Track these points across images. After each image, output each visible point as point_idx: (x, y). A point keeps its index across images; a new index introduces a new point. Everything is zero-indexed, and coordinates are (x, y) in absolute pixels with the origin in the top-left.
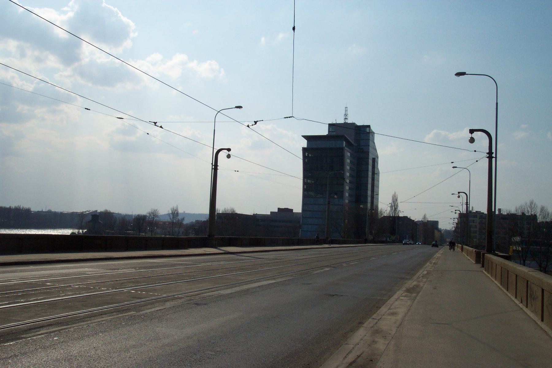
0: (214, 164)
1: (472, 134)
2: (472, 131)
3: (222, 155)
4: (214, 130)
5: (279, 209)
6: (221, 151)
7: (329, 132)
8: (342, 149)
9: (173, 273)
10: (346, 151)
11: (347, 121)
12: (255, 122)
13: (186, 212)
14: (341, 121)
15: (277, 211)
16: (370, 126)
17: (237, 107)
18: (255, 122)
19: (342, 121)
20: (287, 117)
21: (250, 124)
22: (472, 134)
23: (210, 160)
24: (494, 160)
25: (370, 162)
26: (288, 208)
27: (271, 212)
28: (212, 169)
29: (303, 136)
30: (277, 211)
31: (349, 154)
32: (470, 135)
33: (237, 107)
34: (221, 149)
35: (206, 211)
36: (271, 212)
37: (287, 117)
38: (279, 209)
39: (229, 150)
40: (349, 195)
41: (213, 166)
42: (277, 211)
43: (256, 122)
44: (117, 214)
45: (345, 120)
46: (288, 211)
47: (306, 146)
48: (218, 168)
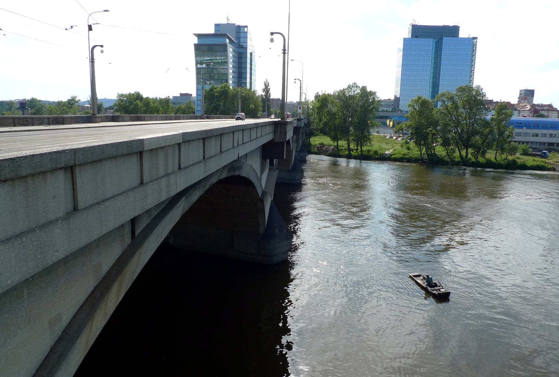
0: (91, 58)
1: (272, 35)
2: (272, 34)
3: (97, 50)
4: (289, 13)
5: (181, 94)
6: (96, 47)
7: (215, 31)
8: (225, 46)
9: (535, 200)
10: (228, 47)
11: (229, 22)
12: (71, 26)
13: (107, 98)
14: (224, 22)
15: (179, 95)
16: (247, 26)
17: (105, 11)
18: (71, 26)
19: (226, 22)
20: (95, 24)
21: (68, 28)
22: (272, 35)
23: (87, 55)
24: (286, 55)
25: (249, 56)
26: (188, 93)
27: (173, 97)
28: (90, 62)
29: (194, 34)
30: (179, 96)
31: (231, 50)
32: (271, 37)
33: (105, 11)
34: (94, 46)
35: (299, 101)
36: (173, 97)
37: (95, 24)
38: (181, 94)
39: (102, 46)
40: (232, 82)
41: (91, 60)
42: (179, 95)
43: (72, 27)
44: (45, 101)
45: (228, 21)
46: (188, 95)
47: (196, 43)
48: (95, 61)
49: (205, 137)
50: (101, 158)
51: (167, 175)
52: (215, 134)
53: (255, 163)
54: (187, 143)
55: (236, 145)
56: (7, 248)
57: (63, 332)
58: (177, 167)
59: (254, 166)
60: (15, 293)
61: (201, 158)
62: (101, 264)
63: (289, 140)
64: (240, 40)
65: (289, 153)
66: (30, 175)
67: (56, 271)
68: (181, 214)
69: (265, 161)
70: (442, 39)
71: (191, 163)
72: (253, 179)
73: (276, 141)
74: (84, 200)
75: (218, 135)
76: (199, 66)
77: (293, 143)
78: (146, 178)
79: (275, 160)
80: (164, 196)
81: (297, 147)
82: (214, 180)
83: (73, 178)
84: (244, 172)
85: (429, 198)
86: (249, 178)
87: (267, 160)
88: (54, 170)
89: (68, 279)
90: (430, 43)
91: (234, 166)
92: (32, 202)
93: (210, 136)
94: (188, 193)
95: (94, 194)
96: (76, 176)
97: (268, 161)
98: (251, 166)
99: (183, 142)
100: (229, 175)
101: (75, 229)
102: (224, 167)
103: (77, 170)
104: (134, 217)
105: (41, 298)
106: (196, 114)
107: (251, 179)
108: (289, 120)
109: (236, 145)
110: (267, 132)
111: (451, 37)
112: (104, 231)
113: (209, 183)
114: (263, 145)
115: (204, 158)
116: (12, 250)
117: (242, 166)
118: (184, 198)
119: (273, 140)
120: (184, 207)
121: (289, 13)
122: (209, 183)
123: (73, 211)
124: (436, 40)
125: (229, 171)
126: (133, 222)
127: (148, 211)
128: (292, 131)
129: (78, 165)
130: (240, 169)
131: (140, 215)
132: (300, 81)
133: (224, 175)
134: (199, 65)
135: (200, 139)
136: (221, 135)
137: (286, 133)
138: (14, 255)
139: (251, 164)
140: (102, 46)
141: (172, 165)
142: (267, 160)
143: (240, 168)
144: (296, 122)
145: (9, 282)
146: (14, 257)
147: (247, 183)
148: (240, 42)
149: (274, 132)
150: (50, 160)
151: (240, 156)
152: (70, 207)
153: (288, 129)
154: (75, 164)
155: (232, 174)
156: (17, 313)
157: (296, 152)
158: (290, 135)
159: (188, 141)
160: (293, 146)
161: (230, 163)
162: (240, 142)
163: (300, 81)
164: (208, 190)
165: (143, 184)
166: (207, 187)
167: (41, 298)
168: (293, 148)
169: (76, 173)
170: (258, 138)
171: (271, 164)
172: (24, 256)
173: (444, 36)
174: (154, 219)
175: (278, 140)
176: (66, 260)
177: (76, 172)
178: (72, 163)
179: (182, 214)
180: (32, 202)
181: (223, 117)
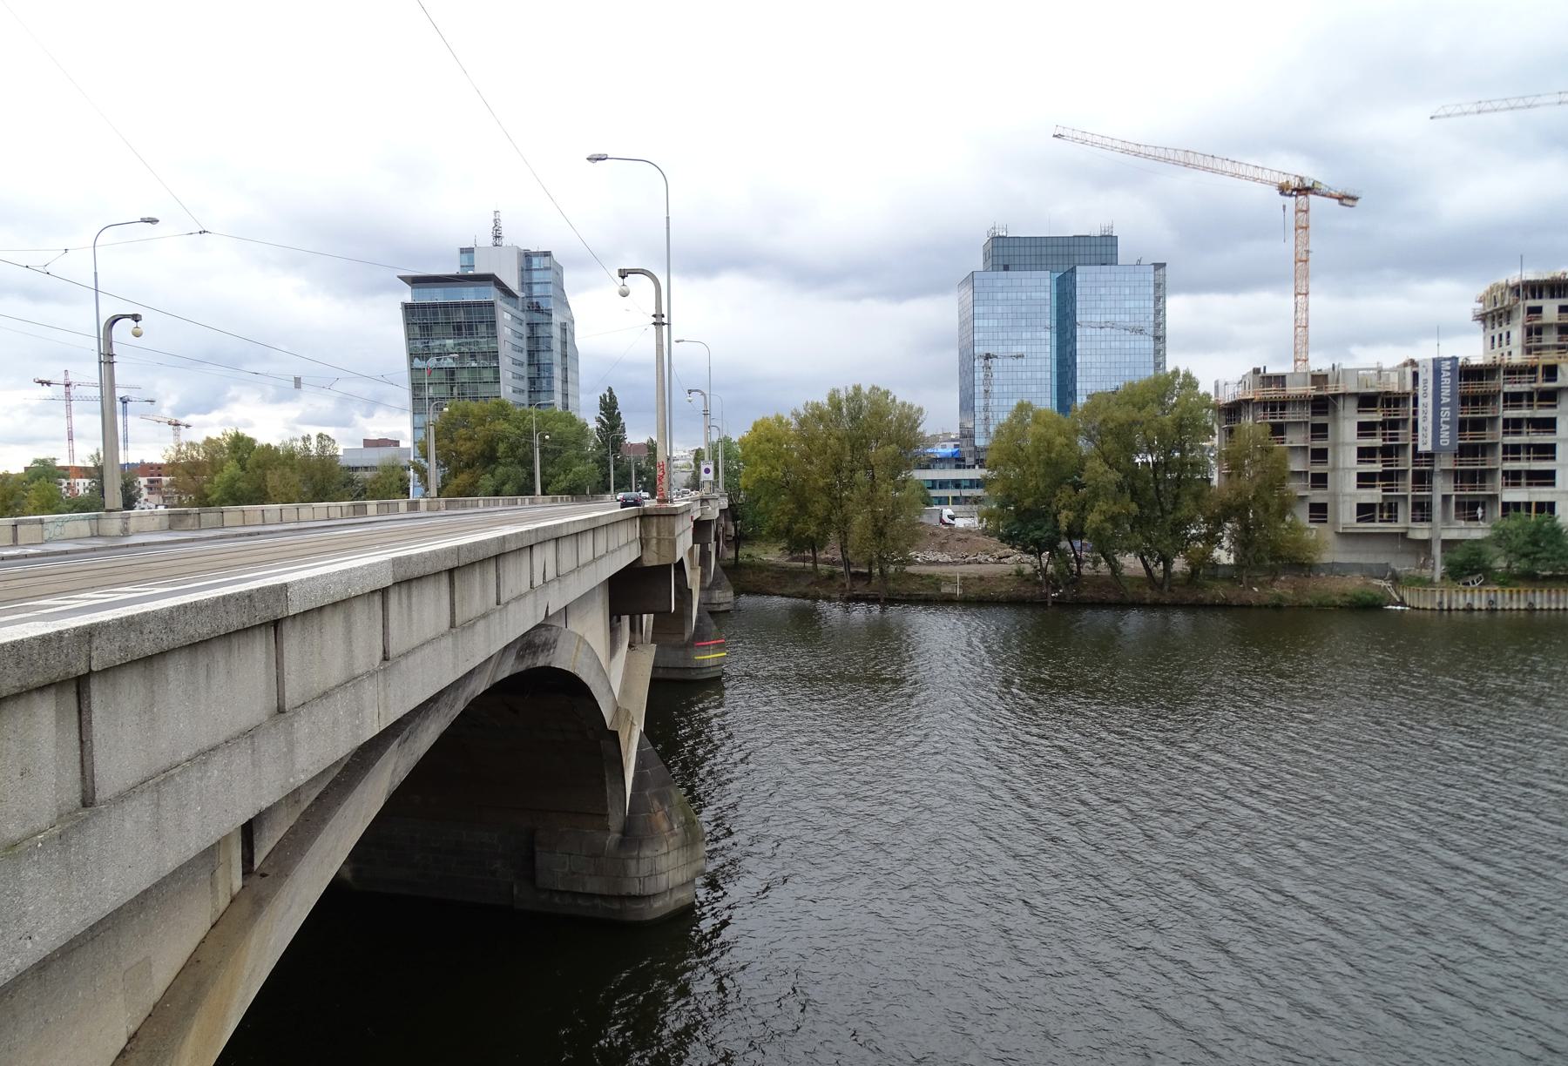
1: (623, 277)
2: (623, 274)
3: (123, 329)
13: (146, 462)
25: (556, 332)
29: (403, 278)
39: (136, 318)
49: (456, 564)
50: (165, 646)
51: (352, 680)
52: (481, 555)
53: (592, 627)
55: (538, 581)
58: (379, 654)
59: (588, 638)
62: (150, 965)
63: (682, 559)
64: (530, 289)
65: (684, 593)
67: (12, 997)
68: (386, 791)
69: (619, 620)
70: (1073, 271)
71: (416, 642)
73: (647, 564)
76: (418, 363)
77: (692, 568)
79: (645, 616)
80: (343, 745)
81: (703, 576)
82: (480, 686)
84: (563, 658)
86: (576, 672)
89: (46, 1022)
90: (1039, 287)
91: (528, 644)
93: (468, 561)
95: (142, 754)
96: (90, 703)
97: (626, 620)
98: (581, 639)
99: (394, 584)
100: (522, 668)
101: (85, 864)
102: (507, 648)
103: (97, 691)
104: (257, 812)
106: (411, 499)
107: (580, 676)
108: (679, 504)
109: (538, 581)
110: (623, 540)
111: (1096, 264)
112: (170, 864)
114: (611, 579)
117: (555, 641)
119: (639, 559)
120: (395, 770)
123: (78, 810)
124: (1057, 275)
125: (520, 657)
126: (249, 831)
127: (294, 795)
128: (690, 533)
130: (549, 650)
131: (269, 809)
132: (703, 394)
133: (506, 671)
134: (416, 360)
135: (439, 573)
136: (497, 557)
137: (673, 544)
139: (580, 633)
140: (136, 318)
141: (366, 654)
143: (548, 646)
144: (697, 506)
147: (571, 688)
148: (530, 296)
150: (18, 663)
151: (550, 613)
153: (678, 530)
154: (91, 671)
155: (528, 663)
157: (702, 589)
159: (409, 581)
160: (693, 578)
161: (524, 635)
162: (551, 574)
163: (703, 394)
165: (284, 712)
166: (460, 706)
173: (1079, 264)
175: (652, 560)
177: (92, 694)
178: (81, 668)
179: (389, 791)
181: (492, 502)
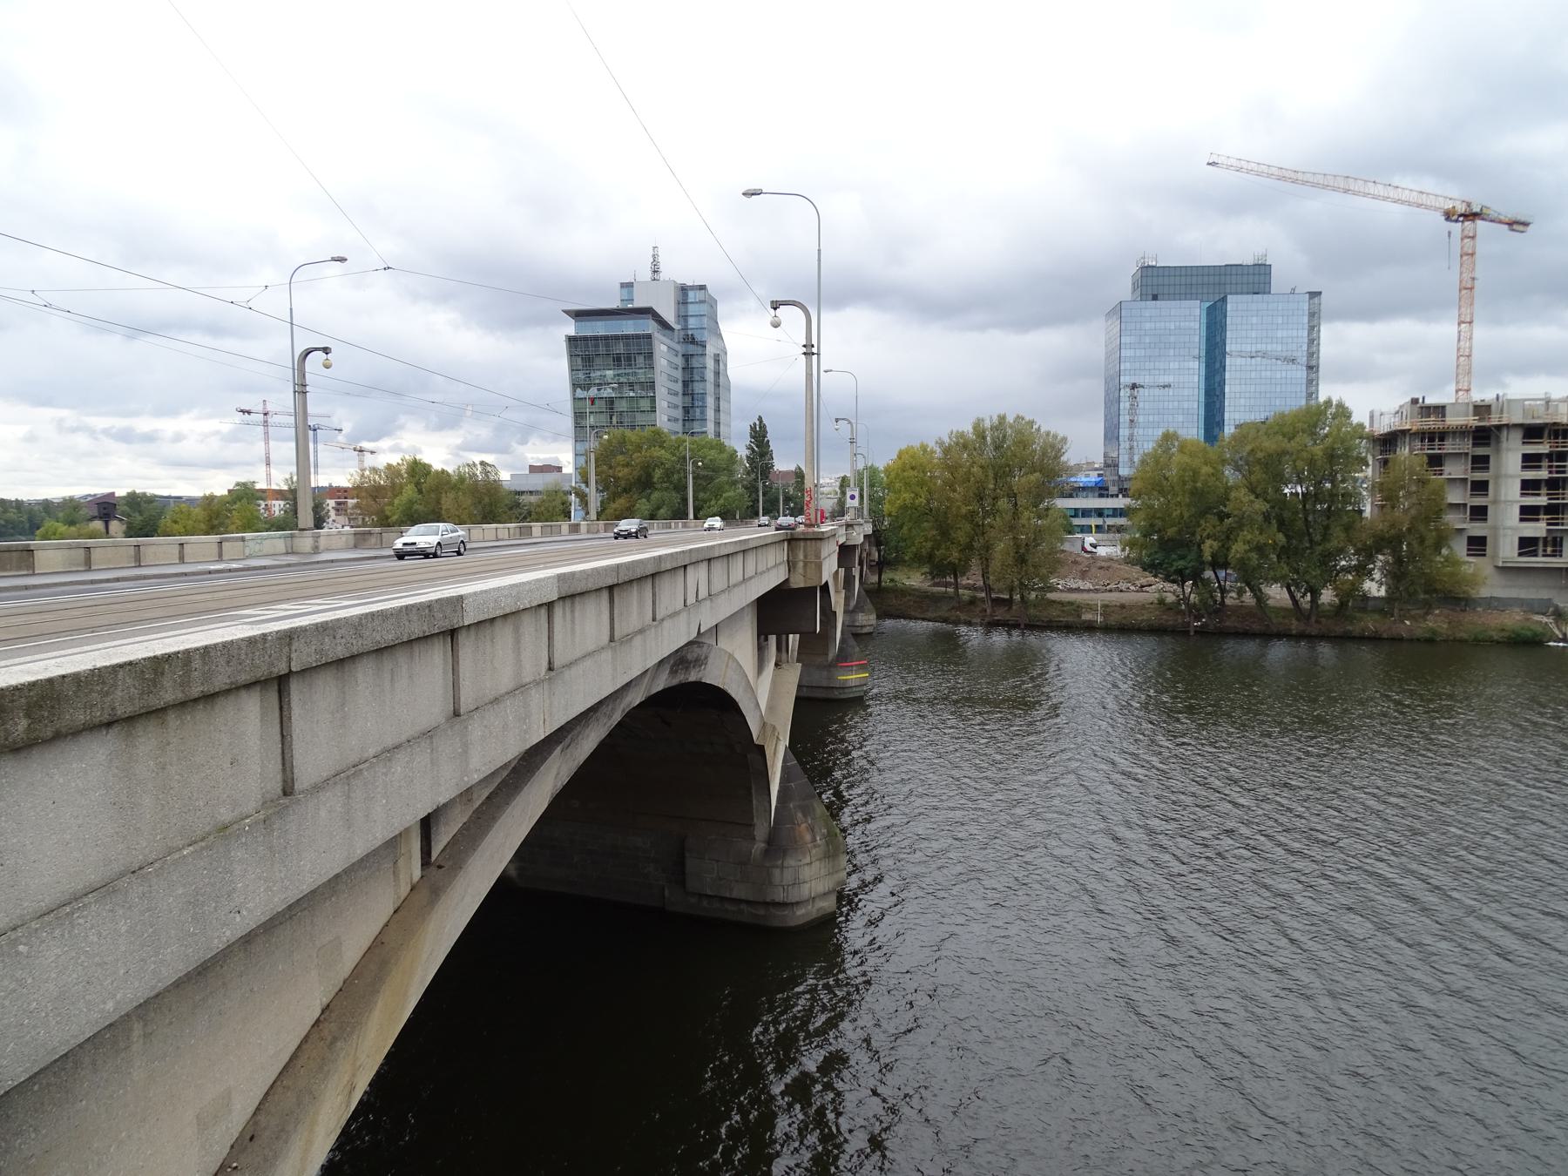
1: (775, 309)
2: (776, 305)
4: (819, 250)
25: (710, 364)
39: (326, 350)
49: (616, 582)
50: (355, 650)
53: (741, 645)
54: (568, 603)
55: (691, 600)
56: (107, 907)
57: (232, 1147)
60: (108, 1036)
61: (606, 638)
63: (827, 582)
65: (829, 615)
66: (174, 706)
67: (222, 967)
72: (736, 692)
74: (308, 769)
75: (647, 576)
76: (580, 393)
77: (837, 591)
78: (466, 702)
79: (791, 636)
80: (512, 749)
81: (847, 599)
82: (636, 698)
83: (281, 708)
84: (712, 675)
85: (1194, 714)
87: (770, 636)
88: (234, 690)
89: (251, 990)
91: (681, 659)
92: (176, 777)
94: (569, 737)
97: (773, 639)
98: (731, 656)
100: (675, 682)
101: (286, 848)
102: (661, 662)
103: (295, 687)
105: (178, 1048)
107: (729, 691)
109: (691, 600)
110: (771, 563)
113: (622, 706)
115: (612, 639)
116: (121, 912)
117: (706, 658)
118: (559, 749)
119: (787, 581)
120: (558, 774)
121: (819, 250)
122: (622, 706)
125: (673, 672)
126: (427, 825)
128: (835, 557)
129: (297, 672)
130: (700, 666)
132: (850, 423)
133: (660, 684)
134: (579, 390)
137: (819, 567)
138: (124, 929)
139: (729, 650)
140: (326, 350)
141: (533, 665)
142: (770, 636)
143: (699, 662)
144: (843, 531)
145: (110, 1005)
146: (126, 932)
147: (720, 703)
148: (685, 328)
149: (788, 561)
151: (702, 631)
152: (276, 786)
153: (824, 554)
155: (680, 678)
156: (111, 1096)
157: (845, 612)
158: (830, 567)
161: (677, 651)
162: (703, 593)
164: (619, 724)
166: (617, 717)
167: (178, 1048)
168: (836, 602)
169: (289, 694)
170: (735, 586)
171: (781, 647)
172: (151, 930)
174: (478, 813)
175: (798, 582)
176: (270, 927)
178: (282, 668)
180: (176, 777)
